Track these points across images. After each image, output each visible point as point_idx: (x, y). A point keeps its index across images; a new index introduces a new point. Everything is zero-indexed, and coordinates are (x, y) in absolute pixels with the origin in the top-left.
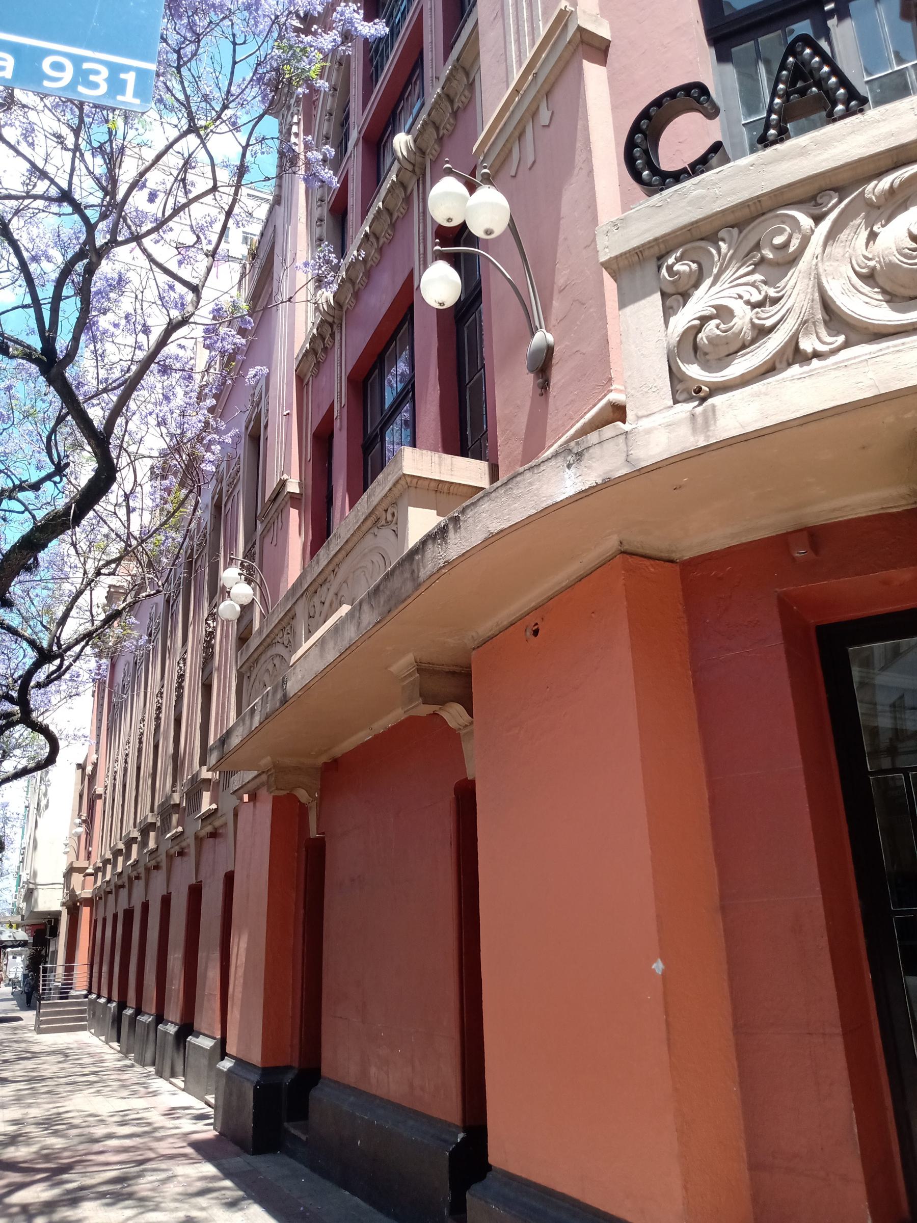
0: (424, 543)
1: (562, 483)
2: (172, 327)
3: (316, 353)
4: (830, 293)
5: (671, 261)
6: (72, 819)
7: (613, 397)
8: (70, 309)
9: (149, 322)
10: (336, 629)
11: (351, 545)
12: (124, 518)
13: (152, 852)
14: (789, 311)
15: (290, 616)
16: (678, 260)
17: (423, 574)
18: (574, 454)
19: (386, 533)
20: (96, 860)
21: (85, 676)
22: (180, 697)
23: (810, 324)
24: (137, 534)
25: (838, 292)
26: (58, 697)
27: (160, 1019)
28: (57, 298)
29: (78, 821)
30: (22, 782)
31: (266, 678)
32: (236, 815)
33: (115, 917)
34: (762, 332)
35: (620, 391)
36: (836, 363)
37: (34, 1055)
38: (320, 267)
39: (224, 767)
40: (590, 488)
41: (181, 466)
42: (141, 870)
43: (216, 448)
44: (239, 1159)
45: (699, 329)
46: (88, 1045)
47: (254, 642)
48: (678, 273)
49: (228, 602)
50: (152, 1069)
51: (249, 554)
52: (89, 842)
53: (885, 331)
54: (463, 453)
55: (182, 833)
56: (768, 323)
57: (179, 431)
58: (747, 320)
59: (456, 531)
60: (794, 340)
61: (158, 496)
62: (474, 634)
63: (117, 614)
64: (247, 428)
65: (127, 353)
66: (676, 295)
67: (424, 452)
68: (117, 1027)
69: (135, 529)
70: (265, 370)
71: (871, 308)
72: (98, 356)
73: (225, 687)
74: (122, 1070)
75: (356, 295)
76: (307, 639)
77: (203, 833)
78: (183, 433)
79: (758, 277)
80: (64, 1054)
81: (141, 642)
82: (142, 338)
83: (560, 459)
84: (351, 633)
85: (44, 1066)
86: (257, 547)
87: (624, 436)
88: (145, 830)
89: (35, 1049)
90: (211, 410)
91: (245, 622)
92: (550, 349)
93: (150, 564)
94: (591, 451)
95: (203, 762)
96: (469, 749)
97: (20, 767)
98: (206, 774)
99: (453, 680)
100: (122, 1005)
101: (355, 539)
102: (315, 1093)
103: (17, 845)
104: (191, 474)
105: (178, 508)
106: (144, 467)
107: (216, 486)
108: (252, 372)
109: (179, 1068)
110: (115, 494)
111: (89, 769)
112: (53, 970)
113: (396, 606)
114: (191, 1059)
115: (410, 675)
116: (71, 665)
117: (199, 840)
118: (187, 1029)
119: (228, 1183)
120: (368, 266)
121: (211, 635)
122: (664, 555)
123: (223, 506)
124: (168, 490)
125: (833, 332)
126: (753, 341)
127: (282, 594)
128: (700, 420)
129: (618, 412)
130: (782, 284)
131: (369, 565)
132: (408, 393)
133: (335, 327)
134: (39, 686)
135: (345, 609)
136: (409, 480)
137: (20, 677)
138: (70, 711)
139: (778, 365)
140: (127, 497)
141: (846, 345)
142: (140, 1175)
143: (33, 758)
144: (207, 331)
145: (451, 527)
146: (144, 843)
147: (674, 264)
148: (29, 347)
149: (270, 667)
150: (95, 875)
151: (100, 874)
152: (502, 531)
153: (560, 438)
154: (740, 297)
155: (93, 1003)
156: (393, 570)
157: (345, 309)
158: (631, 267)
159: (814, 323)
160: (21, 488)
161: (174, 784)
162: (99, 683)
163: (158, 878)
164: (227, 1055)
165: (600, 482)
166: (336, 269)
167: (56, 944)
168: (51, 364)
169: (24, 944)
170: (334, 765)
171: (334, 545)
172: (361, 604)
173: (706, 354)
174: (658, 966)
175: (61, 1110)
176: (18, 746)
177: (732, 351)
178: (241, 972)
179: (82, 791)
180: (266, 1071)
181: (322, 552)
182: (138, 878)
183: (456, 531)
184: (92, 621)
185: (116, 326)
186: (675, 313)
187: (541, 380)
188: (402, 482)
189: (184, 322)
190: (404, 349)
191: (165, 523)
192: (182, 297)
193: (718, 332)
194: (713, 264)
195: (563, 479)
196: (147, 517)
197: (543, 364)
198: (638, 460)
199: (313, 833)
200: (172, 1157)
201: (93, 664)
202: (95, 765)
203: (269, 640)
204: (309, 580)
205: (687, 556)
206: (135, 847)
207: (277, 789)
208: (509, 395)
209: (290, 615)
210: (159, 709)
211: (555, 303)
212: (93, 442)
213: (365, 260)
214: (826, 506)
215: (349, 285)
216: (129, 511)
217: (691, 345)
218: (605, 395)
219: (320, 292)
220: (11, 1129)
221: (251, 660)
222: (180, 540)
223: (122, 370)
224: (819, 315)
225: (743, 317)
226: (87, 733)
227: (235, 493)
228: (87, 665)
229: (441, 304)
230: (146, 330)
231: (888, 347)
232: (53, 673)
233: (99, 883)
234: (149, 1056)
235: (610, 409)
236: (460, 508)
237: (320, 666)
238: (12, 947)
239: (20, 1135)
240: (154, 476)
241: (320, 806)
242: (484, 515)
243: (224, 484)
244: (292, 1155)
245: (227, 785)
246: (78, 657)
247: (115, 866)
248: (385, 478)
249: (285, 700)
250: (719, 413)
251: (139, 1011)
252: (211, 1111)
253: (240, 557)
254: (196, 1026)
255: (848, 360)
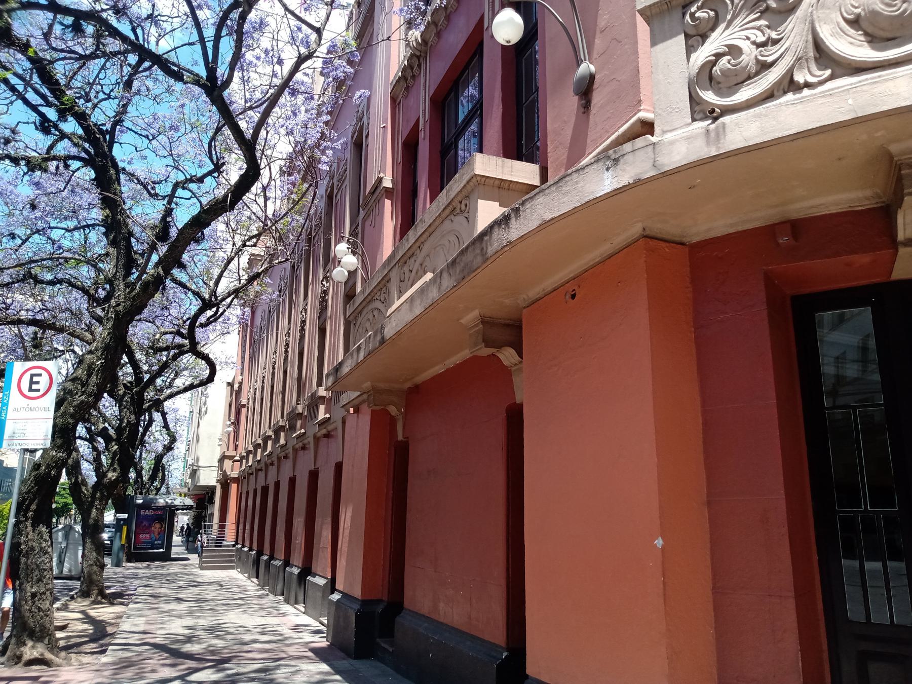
0: (491, 227)
1: (603, 182)
2: (301, 60)
3: (406, 80)
4: (822, 35)
5: (693, 9)
6: (224, 422)
7: (642, 115)
8: (227, 46)
9: (283, 56)
10: (422, 290)
11: (433, 228)
12: (262, 205)
13: (282, 446)
14: (787, 50)
15: (386, 280)
16: (699, 9)
17: (491, 250)
18: (611, 158)
19: (460, 219)
20: (242, 450)
21: (234, 320)
22: (302, 337)
23: (804, 61)
24: (270, 216)
25: (826, 34)
26: (215, 334)
27: (287, 563)
28: (217, 38)
29: (229, 423)
30: (188, 394)
31: (368, 325)
32: (344, 422)
33: (255, 491)
34: (764, 67)
35: (648, 111)
36: (823, 92)
37: (199, 584)
38: (411, 14)
39: (337, 388)
40: (624, 186)
41: (303, 164)
42: (275, 459)
43: (329, 152)
44: (344, 662)
45: (714, 63)
46: (236, 579)
47: (359, 300)
48: (699, 18)
49: (339, 269)
50: (281, 598)
51: (353, 233)
52: (236, 438)
53: (864, 66)
54: (519, 157)
55: (304, 433)
56: (770, 59)
57: (303, 140)
58: (753, 56)
59: (516, 219)
60: (790, 74)
61: (285, 188)
62: (525, 296)
63: (257, 276)
64: (352, 137)
65: (266, 81)
66: (696, 36)
67: (491, 157)
68: (256, 568)
69: (270, 213)
70: (368, 93)
71: (850, 46)
72: (245, 81)
73: (335, 331)
74: (260, 597)
75: (438, 34)
76: (399, 298)
77: (319, 434)
78: (306, 141)
79: (763, 22)
80: (220, 585)
81: (274, 296)
82: (277, 68)
83: (601, 164)
84: (434, 294)
85: (206, 592)
86: (360, 228)
87: (652, 147)
88: (278, 430)
89: (200, 580)
90: (326, 123)
91: (351, 283)
92: (592, 77)
93: (280, 239)
94: (626, 157)
95: (319, 384)
96: (516, 380)
97: (187, 383)
98: (322, 392)
99: (508, 330)
100: (260, 553)
101: (436, 223)
102: (399, 619)
103: (184, 438)
104: (310, 172)
105: (301, 198)
106: (275, 168)
107: (329, 182)
108: (358, 94)
109: (301, 598)
110: (256, 188)
111: (236, 386)
112: (210, 527)
113: (469, 274)
114: (310, 593)
115: (476, 325)
116: (225, 311)
117: (317, 439)
118: (307, 571)
119: (338, 677)
120: (448, 12)
121: (325, 292)
122: (677, 239)
123: (336, 197)
124: (294, 184)
125: (822, 66)
126: (757, 73)
127: (379, 265)
128: (713, 135)
129: (647, 127)
130: (782, 28)
131: (447, 243)
132: (477, 111)
133: (421, 59)
134: (202, 326)
135: (429, 276)
136: (479, 178)
137: (188, 319)
138: (224, 344)
139: (776, 93)
140: (264, 189)
141: (832, 77)
142: (278, 667)
143: (196, 377)
144: (325, 63)
145: (513, 215)
146: (277, 439)
147: (696, 12)
148: (197, 75)
149: (371, 317)
150: (240, 461)
151: (244, 461)
152: (553, 219)
153: (597, 147)
154: (748, 38)
155: (239, 550)
156: (467, 248)
157: (429, 45)
158: (661, 13)
159: (807, 60)
160: (191, 180)
161: (298, 400)
162: (243, 325)
163: (287, 466)
164: (336, 590)
165: (631, 182)
166: (424, 14)
167: (213, 508)
168: (214, 88)
169: (189, 508)
170: (416, 390)
171: (420, 228)
172: (441, 272)
173: (719, 83)
174: (659, 542)
175: (221, 622)
176: (186, 369)
177: (739, 81)
178: (347, 532)
179: (231, 401)
180: (364, 603)
181: (411, 232)
182: (272, 464)
183: (516, 219)
184: (240, 280)
185: (258, 58)
186: (695, 51)
187: (584, 102)
188: (474, 180)
189: (310, 56)
190: (474, 77)
191: (292, 209)
192: (307, 36)
193: (729, 66)
194: (727, 12)
195: (603, 180)
196: (278, 202)
197: (586, 90)
198: (663, 165)
199: (400, 437)
200: (299, 658)
201: (238, 312)
202: (241, 384)
203: (370, 297)
204: (401, 254)
205: (695, 239)
206: (270, 443)
207: (375, 405)
208: (558, 114)
209: (386, 279)
210: (287, 345)
211: (597, 41)
212: (243, 147)
213: (446, 7)
214: (806, 204)
215: (433, 27)
216: (266, 199)
217: (707, 76)
218: (635, 114)
219: (411, 32)
220: (187, 632)
221: (357, 312)
222: (302, 221)
223: (262, 92)
224: (811, 53)
225: (750, 54)
226: (235, 360)
227: (343, 187)
228: (235, 313)
229: (508, 42)
230: (280, 62)
231: (867, 79)
232: (211, 317)
233: (243, 467)
234: (279, 588)
235: (640, 125)
236: (520, 201)
237: (409, 317)
238: (182, 509)
239: (194, 636)
240: (282, 172)
241: (405, 418)
242: (539, 207)
243: (335, 179)
244: (382, 660)
245: (337, 401)
246: (229, 306)
247: (255, 455)
248: (461, 177)
249: (383, 341)
250: (728, 130)
251: (272, 557)
252: (324, 629)
253: (347, 235)
254: (313, 570)
255: (833, 89)
